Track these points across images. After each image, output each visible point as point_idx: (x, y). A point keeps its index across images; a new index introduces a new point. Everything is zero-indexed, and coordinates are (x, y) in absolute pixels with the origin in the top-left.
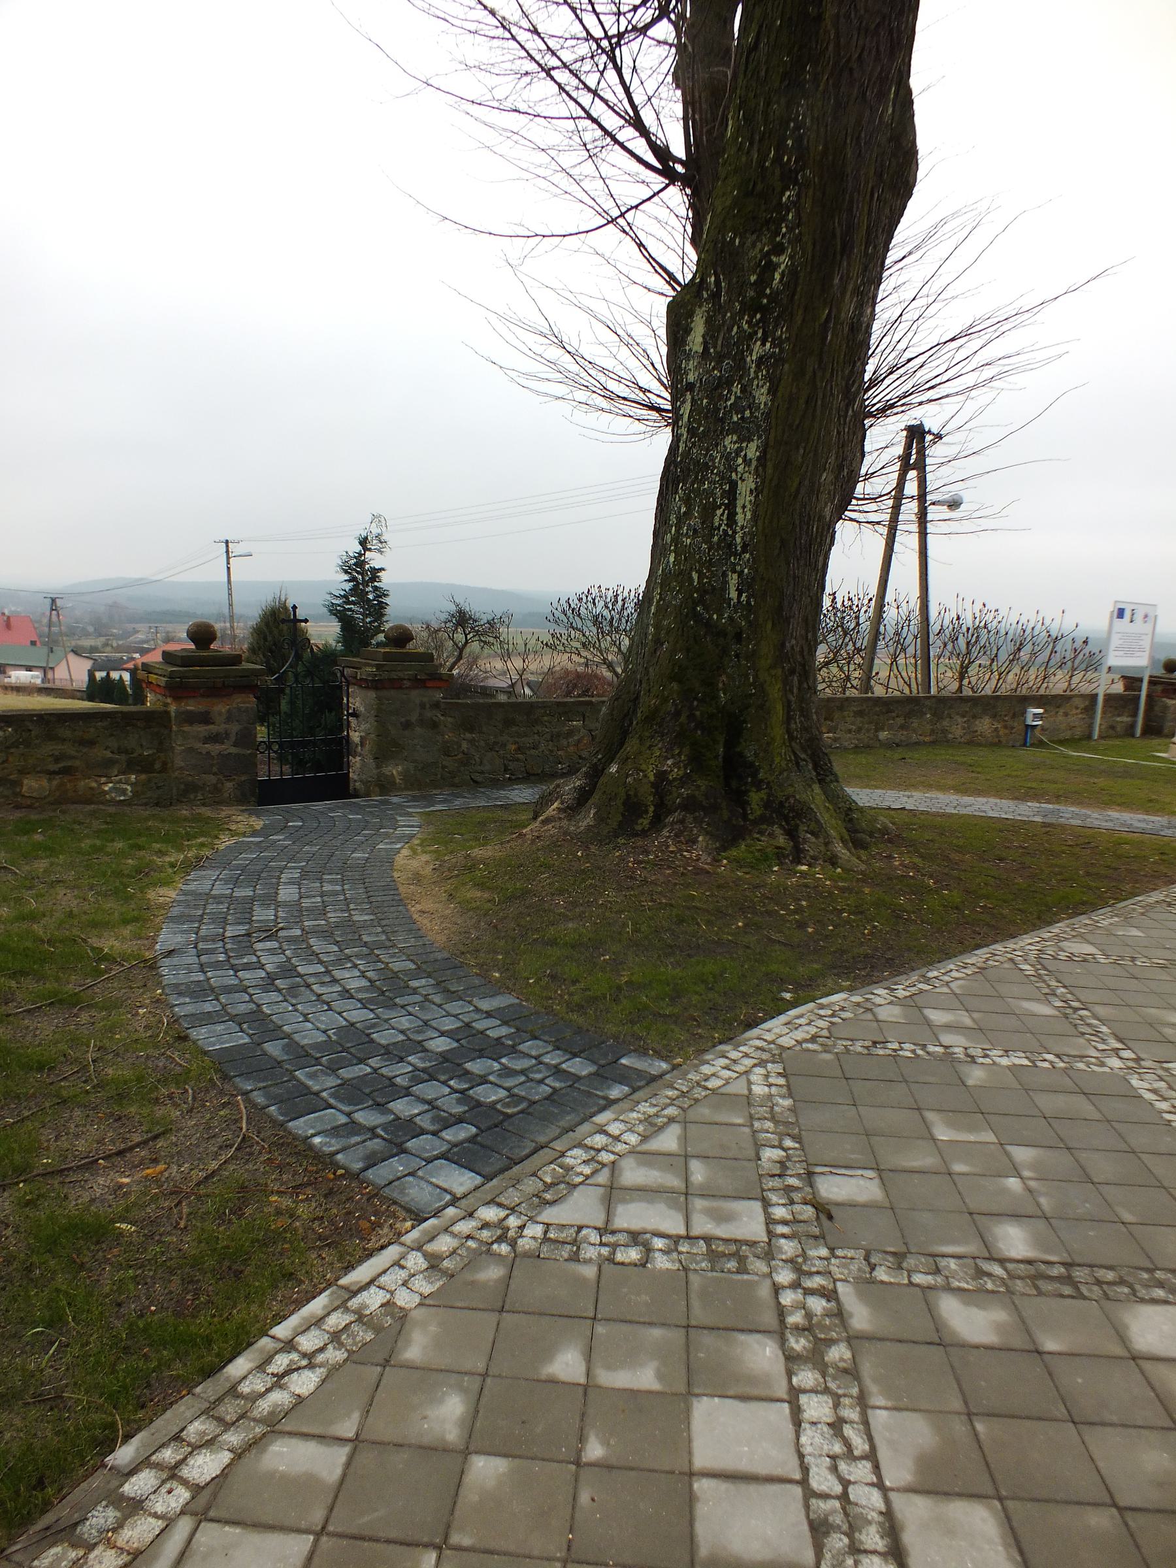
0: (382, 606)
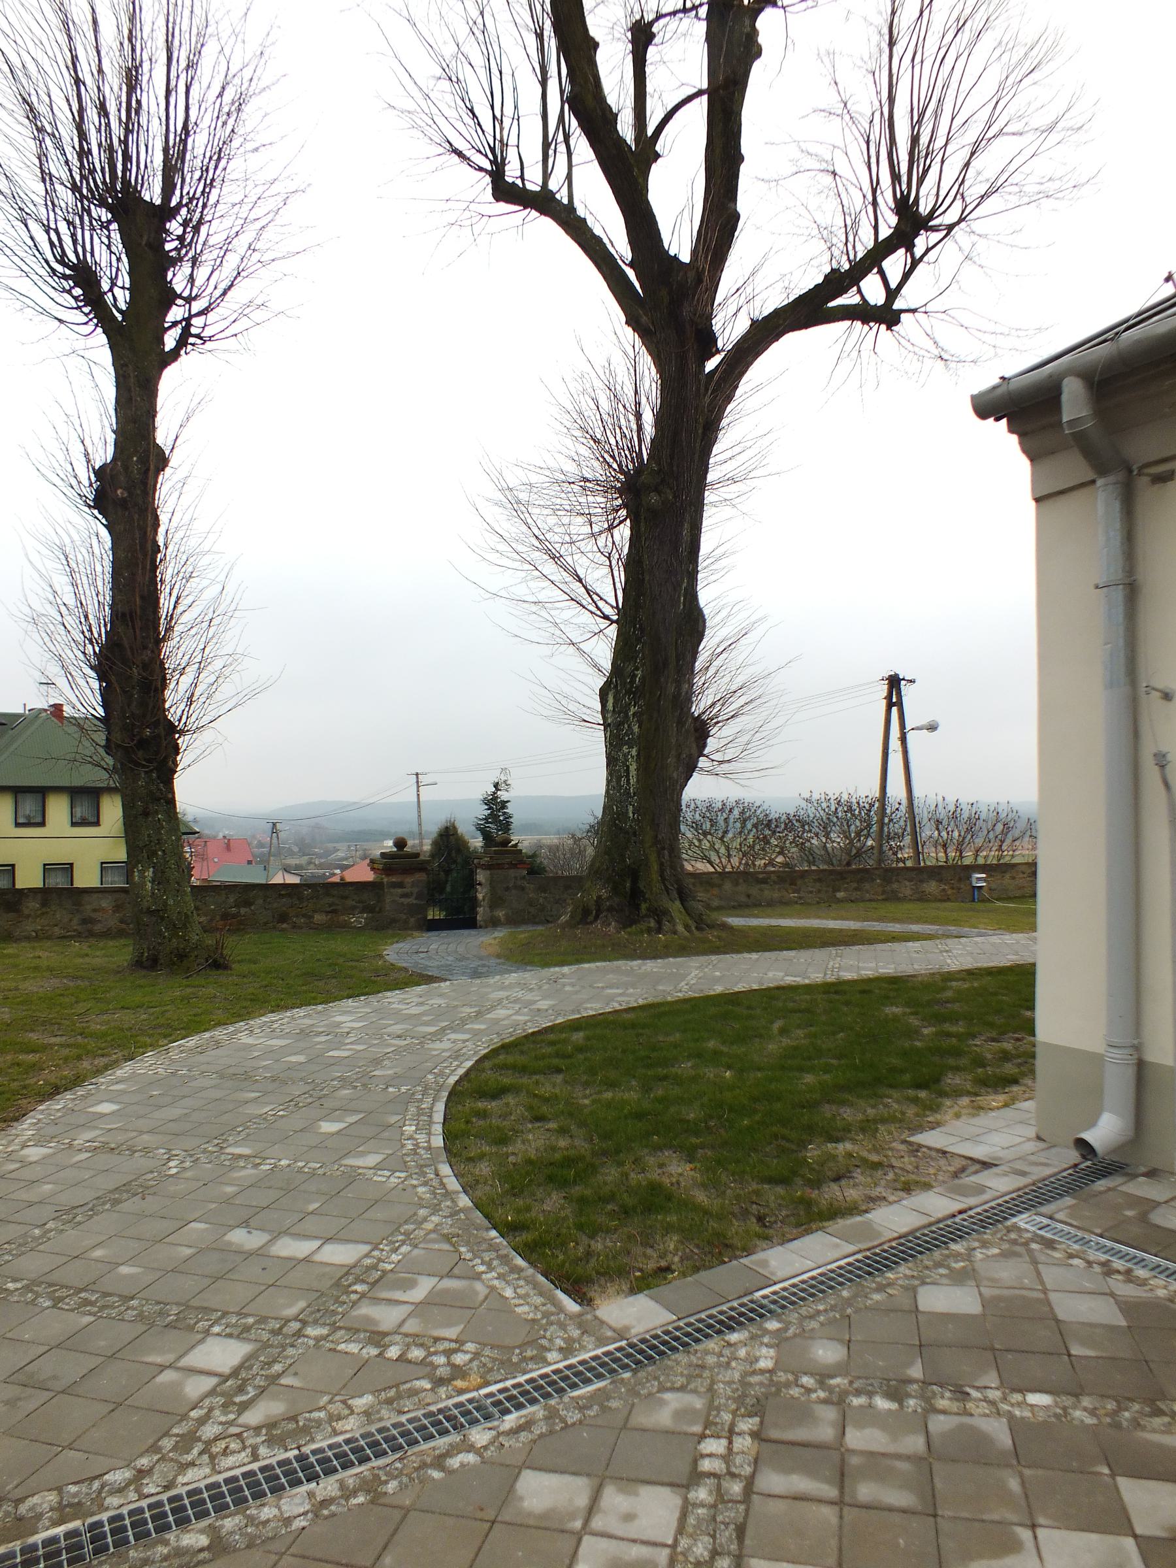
0: (508, 824)
